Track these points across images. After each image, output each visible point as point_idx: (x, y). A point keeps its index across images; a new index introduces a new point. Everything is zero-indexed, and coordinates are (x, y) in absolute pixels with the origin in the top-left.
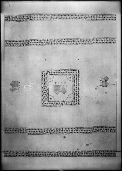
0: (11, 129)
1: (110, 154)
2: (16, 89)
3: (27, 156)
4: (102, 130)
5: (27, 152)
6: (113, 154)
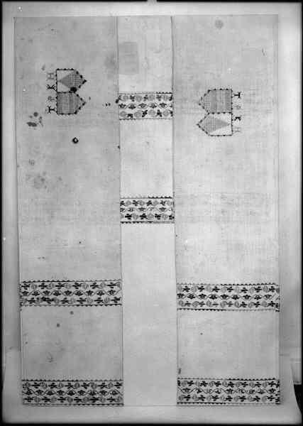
0: (204, 292)
1: (97, 396)
2: (223, 124)
3: (271, 398)
4: (61, 297)
5: (272, 384)
6: (109, 396)
